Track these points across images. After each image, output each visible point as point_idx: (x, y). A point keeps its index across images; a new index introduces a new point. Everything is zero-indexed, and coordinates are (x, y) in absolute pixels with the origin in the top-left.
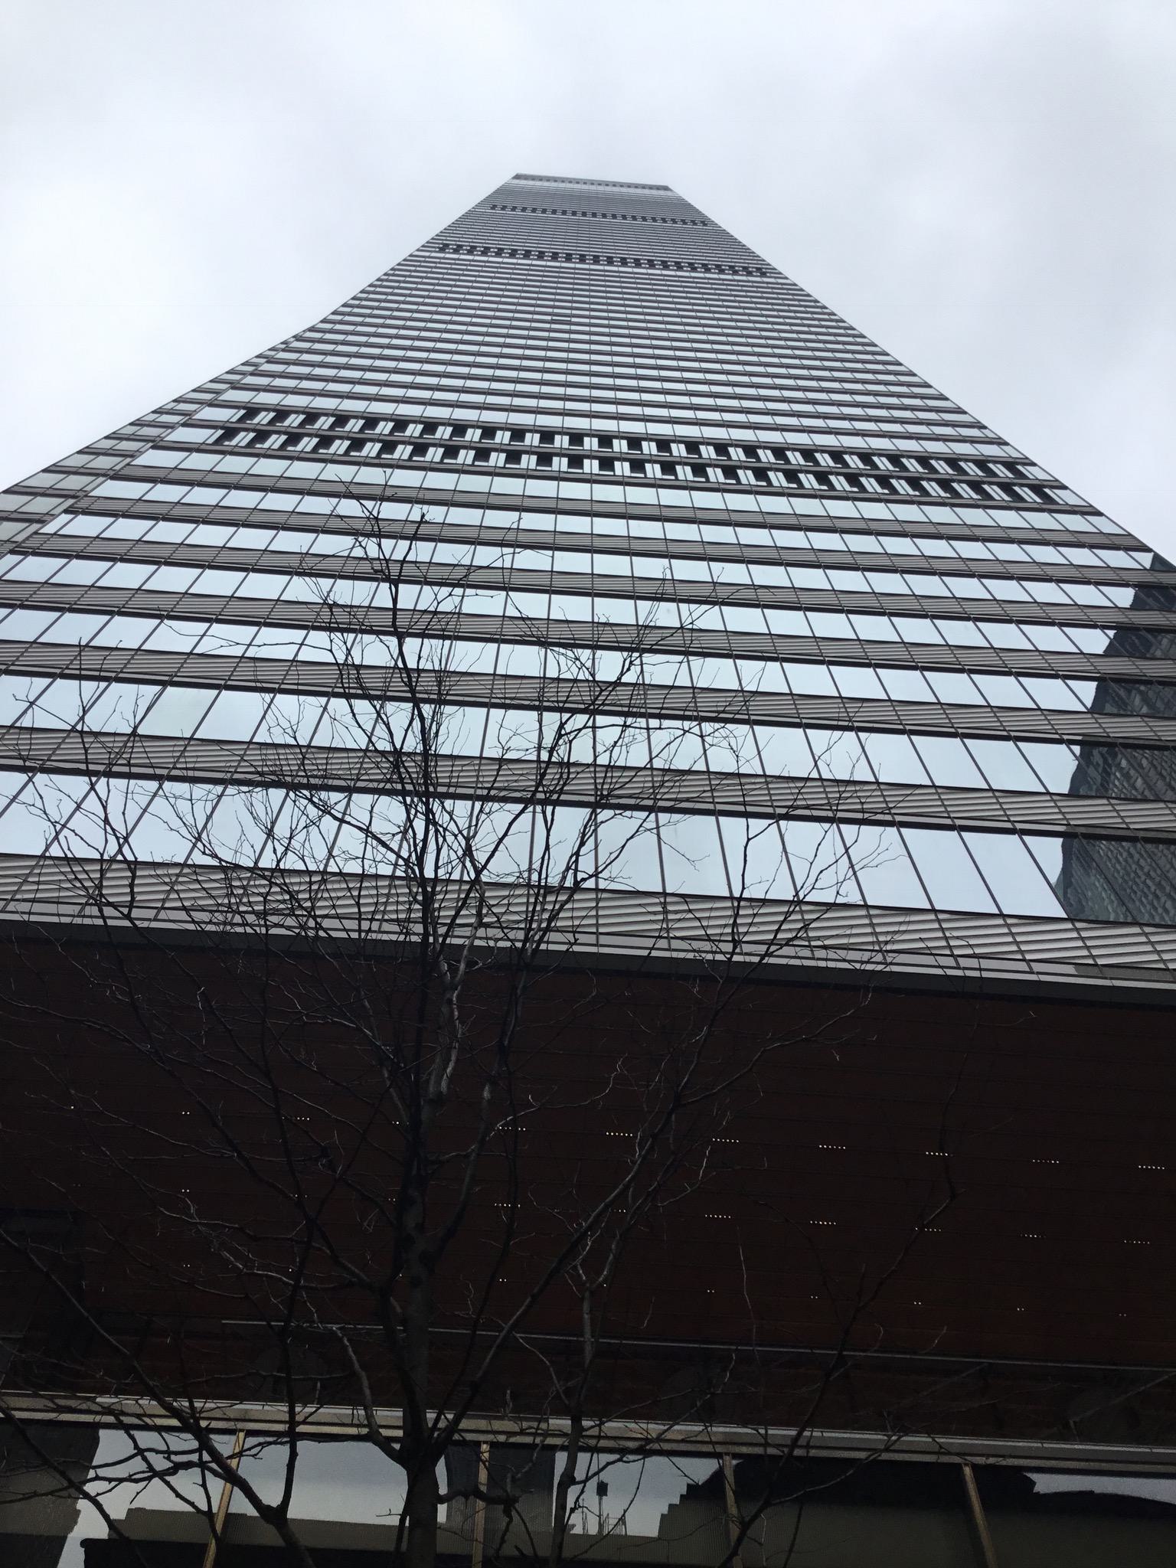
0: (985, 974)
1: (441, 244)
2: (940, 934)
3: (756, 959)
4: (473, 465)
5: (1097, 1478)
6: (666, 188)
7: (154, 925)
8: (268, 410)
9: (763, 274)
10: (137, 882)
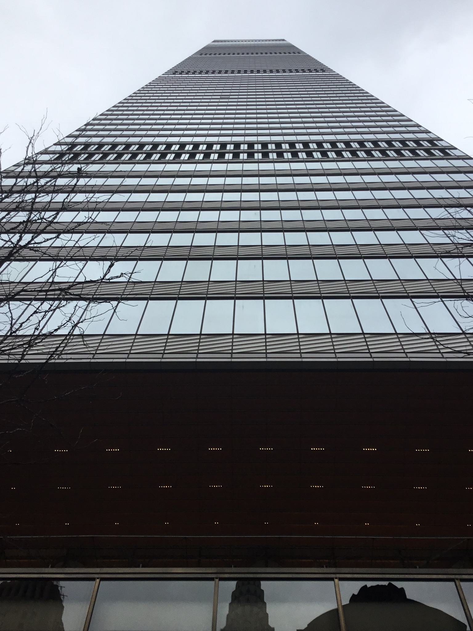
0: (375, 360)
1: (174, 71)
2: (399, 344)
3: (17, 362)
5: (199, 582)
6: (284, 40)
7: (128, 360)
8: (108, 145)
9: (324, 71)
10: (268, 348)
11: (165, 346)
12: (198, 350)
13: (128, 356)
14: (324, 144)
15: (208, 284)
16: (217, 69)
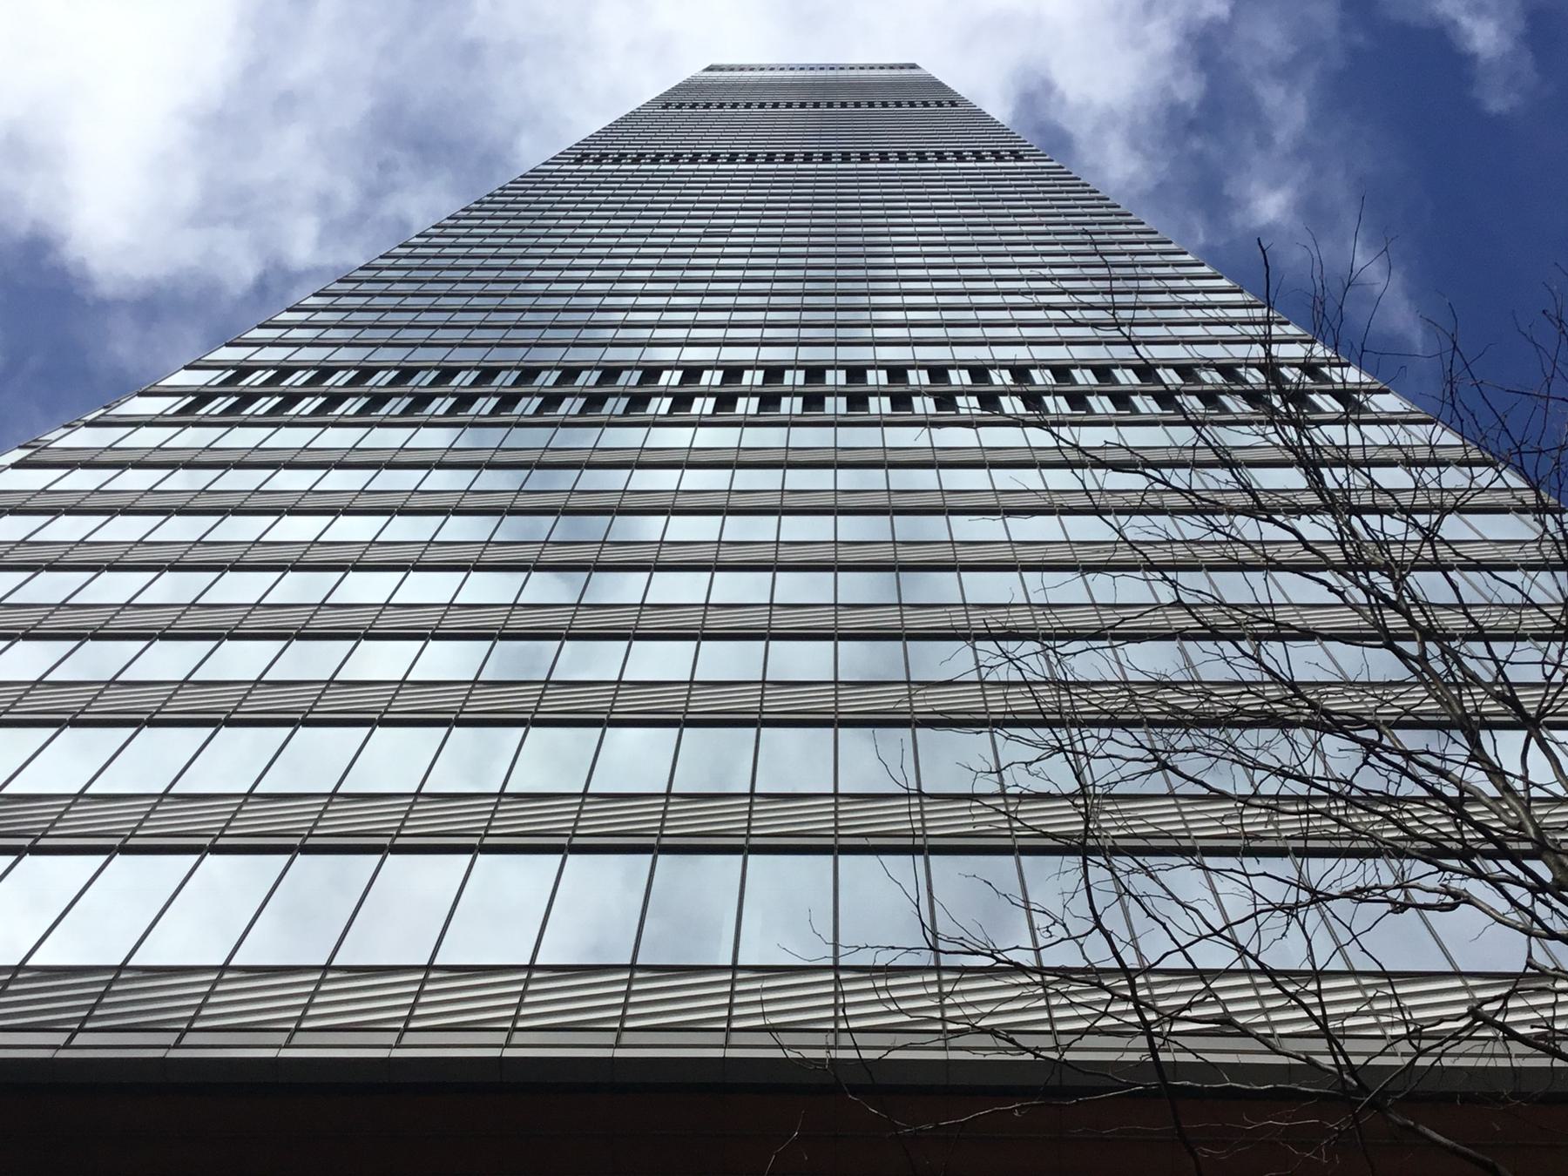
0: (866, 1055)
4: (757, 415)
6: (913, 66)
7: (508, 1053)
11: (519, 1006)
12: (623, 1018)
13: (509, 1038)
14: (1076, 373)
15: (666, 805)
16: (723, 149)
